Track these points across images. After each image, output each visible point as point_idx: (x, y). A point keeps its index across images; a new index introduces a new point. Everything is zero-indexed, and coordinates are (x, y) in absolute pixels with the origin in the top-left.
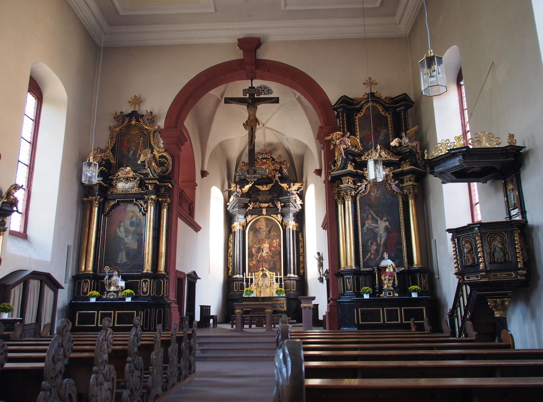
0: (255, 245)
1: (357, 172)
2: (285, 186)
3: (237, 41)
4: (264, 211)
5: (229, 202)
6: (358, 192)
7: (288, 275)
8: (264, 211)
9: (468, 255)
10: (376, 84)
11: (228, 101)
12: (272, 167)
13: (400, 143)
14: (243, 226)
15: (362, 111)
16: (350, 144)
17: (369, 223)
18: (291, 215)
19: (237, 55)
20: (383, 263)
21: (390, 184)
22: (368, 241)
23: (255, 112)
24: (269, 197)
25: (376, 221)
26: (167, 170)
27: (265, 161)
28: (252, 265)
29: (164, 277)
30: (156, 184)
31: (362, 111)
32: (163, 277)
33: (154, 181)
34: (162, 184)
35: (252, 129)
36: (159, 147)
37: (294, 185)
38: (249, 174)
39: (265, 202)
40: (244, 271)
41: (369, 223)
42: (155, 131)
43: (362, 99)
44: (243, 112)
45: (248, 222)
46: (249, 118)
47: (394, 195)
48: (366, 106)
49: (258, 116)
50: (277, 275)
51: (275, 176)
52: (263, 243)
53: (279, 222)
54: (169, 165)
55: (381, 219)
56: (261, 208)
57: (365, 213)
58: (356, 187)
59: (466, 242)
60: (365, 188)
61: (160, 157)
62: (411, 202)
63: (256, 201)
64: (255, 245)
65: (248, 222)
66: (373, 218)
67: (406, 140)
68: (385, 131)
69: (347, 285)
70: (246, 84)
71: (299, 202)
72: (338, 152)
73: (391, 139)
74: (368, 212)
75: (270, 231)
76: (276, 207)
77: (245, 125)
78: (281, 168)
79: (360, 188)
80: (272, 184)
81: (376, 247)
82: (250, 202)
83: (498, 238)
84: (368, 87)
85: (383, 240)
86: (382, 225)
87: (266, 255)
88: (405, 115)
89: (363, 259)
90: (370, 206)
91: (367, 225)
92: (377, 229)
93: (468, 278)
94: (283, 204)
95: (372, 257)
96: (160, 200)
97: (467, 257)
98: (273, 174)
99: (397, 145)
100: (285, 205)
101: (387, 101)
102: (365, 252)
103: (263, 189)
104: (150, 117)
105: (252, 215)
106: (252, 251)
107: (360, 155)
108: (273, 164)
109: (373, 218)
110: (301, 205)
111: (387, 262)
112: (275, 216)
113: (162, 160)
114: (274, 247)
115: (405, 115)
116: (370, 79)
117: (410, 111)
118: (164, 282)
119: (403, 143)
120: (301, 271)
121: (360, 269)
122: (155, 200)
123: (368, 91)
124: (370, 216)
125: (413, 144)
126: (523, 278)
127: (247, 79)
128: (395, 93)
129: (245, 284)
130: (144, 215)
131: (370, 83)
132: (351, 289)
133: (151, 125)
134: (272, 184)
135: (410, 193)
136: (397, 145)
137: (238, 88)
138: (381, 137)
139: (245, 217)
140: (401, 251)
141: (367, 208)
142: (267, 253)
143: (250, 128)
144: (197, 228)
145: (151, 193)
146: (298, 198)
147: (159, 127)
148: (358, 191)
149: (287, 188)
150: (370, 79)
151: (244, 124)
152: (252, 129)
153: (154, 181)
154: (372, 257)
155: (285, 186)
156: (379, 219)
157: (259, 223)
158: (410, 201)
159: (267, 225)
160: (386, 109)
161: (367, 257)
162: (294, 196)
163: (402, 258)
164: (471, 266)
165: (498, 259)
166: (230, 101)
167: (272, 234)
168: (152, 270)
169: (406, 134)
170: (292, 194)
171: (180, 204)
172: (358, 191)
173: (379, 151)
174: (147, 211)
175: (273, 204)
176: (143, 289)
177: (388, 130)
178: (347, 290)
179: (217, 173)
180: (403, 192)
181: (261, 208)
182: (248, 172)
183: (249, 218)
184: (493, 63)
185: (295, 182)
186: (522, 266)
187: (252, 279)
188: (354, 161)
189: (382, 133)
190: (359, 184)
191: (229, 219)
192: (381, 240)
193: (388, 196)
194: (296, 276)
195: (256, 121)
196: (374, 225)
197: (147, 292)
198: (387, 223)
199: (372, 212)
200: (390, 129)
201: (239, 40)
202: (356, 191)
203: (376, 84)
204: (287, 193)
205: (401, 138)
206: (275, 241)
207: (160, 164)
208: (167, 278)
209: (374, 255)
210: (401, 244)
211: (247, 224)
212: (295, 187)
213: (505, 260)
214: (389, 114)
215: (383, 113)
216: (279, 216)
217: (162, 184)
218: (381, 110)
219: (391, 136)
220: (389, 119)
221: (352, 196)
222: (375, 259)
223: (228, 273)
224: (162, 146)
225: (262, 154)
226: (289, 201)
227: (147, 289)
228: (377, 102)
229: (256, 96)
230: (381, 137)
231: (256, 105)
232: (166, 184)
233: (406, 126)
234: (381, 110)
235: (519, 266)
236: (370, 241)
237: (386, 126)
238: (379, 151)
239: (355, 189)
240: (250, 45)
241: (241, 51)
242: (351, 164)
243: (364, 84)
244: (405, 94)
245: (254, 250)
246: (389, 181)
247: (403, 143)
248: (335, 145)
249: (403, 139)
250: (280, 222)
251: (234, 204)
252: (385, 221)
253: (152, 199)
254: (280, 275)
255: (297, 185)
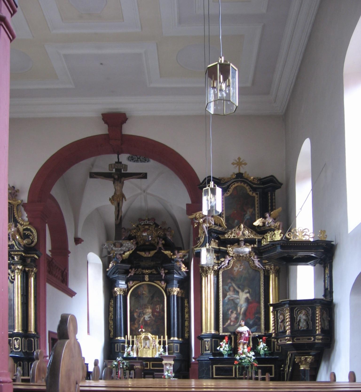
0: (137, 310)
1: (219, 249)
2: (167, 252)
3: (101, 116)
4: (147, 278)
5: (108, 267)
6: (221, 267)
7: (172, 339)
8: (147, 278)
9: (281, 324)
10: (245, 164)
11: (93, 175)
12: (155, 234)
13: (264, 223)
14: (124, 292)
15: (229, 191)
16: (213, 223)
17: (230, 295)
18: (175, 282)
19: (101, 129)
20: (240, 329)
21: (253, 260)
22: (228, 310)
23: (122, 188)
24: (152, 263)
25: (238, 293)
26: (33, 242)
27: (147, 227)
28: (134, 328)
29: (34, 337)
30: (21, 255)
31: (229, 191)
32: (33, 336)
33: (20, 253)
34: (29, 255)
35: (118, 204)
36: (23, 220)
37: (178, 252)
38: (116, 247)
39: (148, 268)
40: (126, 333)
41: (230, 295)
42: (18, 205)
43: (231, 179)
44: (108, 188)
45: (129, 287)
46: (115, 193)
47: (256, 270)
48: (234, 186)
49: (124, 191)
50: (160, 338)
51: (158, 243)
52: (145, 308)
53: (162, 288)
54: (34, 237)
55: (243, 291)
56: (144, 274)
57: (227, 285)
58: (220, 262)
59: (281, 314)
60: (228, 263)
61: (24, 230)
62: (272, 277)
63: (137, 267)
64: (137, 310)
65: (129, 287)
66: (234, 290)
67: (269, 220)
68: (251, 210)
69: (205, 347)
70: (113, 158)
71: (184, 269)
72: (202, 230)
73: (257, 218)
74: (230, 285)
75: (152, 297)
76: (159, 273)
77: (112, 200)
78: (165, 235)
79: (223, 264)
80: (156, 251)
81: (236, 315)
82: (131, 268)
83: (303, 312)
84: (236, 161)
85: (243, 310)
86: (243, 297)
87: (148, 319)
88: (271, 196)
89: (223, 325)
90: (233, 279)
91: (228, 296)
92: (238, 300)
93: (280, 341)
94: (166, 271)
95: (232, 323)
96: (27, 269)
97: (281, 325)
98: (156, 240)
99: (261, 224)
100: (170, 272)
101: (256, 182)
102: (225, 319)
103: (145, 256)
104: (13, 192)
105: (133, 281)
106: (133, 315)
107: (224, 233)
108: (157, 231)
109: (234, 290)
110: (186, 272)
111: (244, 329)
112: (158, 282)
113: (27, 232)
114: (157, 312)
115: (271, 196)
116: (239, 159)
117: (278, 192)
118: (34, 340)
119: (267, 223)
120: (186, 335)
121: (219, 334)
122: (21, 270)
123: (237, 171)
124: (232, 289)
125: (276, 224)
126: (320, 341)
127: (114, 152)
128: (264, 174)
129: (126, 345)
130: (12, 282)
131: (239, 163)
132: (209, 350)
133: (14, 199)
134: (156, 251)
135: (271, 269)
136: (261, 224)
137: (105, 162)
138: (247, 216)
139: (126, 283)
140: (260, 319)
141: (229, 281)
142: (150, 317)
143: (116, 203)
144: (72, 294)
145: (17, 263)
146: (183, 266)
147: (22, 201)
148: (221, 266)
149: (171, 256)
150: (239, 159)
151: (110, 199)
152: (118, 204)
153: (20, 253)
154: (232, 323)
155: (167, 252)
156: (240, 291)
157: (141, 289)
158: (271, 276)
159: (150, 292)
160: (254, 190)
161: (227, 324)
162: (178, 264)
163: (260, 325)
164: (282, 332)
165: (301, 327)
166: (95, 176)
167: (155, 299)
168: (23, 330)
169: (270, 216)
170: (177, 261)
171: (50, 272)
172: (221, 266)
173: (242, 230)
174: (14, 279)
175: (157, 270)
176: (15, 345)
177: (255, 210)
178: (206, 350)
179: (94, 238)
180: (265, 268)
181: (144, 274)
182: (115, 245)
183: (131, 284)
184: (325, 164)
185: (179, 249)
186: (320, 333)
187: (133, 342)
188: (218, 238)
189: (248, 212)
190: (223, 260)
191: (109, 284)
192: (241, 310)
193: (250, 271)
194: (180, 340)
195: (123, 196)
196: (235, 296)
197: (18, 348)
198: (248, 295)
199: (234, 285)
200: (257, 209)
201: (102, 114)
202: (219, 266)
203: (245, 164)
204: (170, 260)
205: (265, 218)
206: (158, 306)
207: (24, 236)
208: (38, 338)
209: (234, 322)
210: (260, 313)
211: (128, 290)
212: (178, 255)
213: (307, 328)
214: (257, 194)
215: (251, 193)
216: (163, 282)
217: (29, 255)
218: (248, 190)
219: (257, 215)
220: (256, 199)
221: (215, 271)
222: (234, 325)
223: (110, 335)
224: (26, 219)
225: (144, 220)
226: (173, 268)
227: (19, 346)
228: (245, 182)
229: (123, 172)
230: (247, 216)
231: (122, 180)
232: (33, 255)
233: (272, 206)
234: (248, 190)
235: (317, 333)
236: (230, 311)
237: (253, 206)
238: (242, 230)
239: (218, 263)
240: (115, 120)
241: (106, 126)
242: (215, 241)
243: (233, 164)
244: (272, 176)
245: (135, 315)
246: (252, 258)
247: (267, 223)
248: (199, 224)
249: (267, 219)
250: (164, 288)
251: (114, 271)
252: (246, 293)
253: (18, 269)
254: (164, 338)
255: (181, 253)
